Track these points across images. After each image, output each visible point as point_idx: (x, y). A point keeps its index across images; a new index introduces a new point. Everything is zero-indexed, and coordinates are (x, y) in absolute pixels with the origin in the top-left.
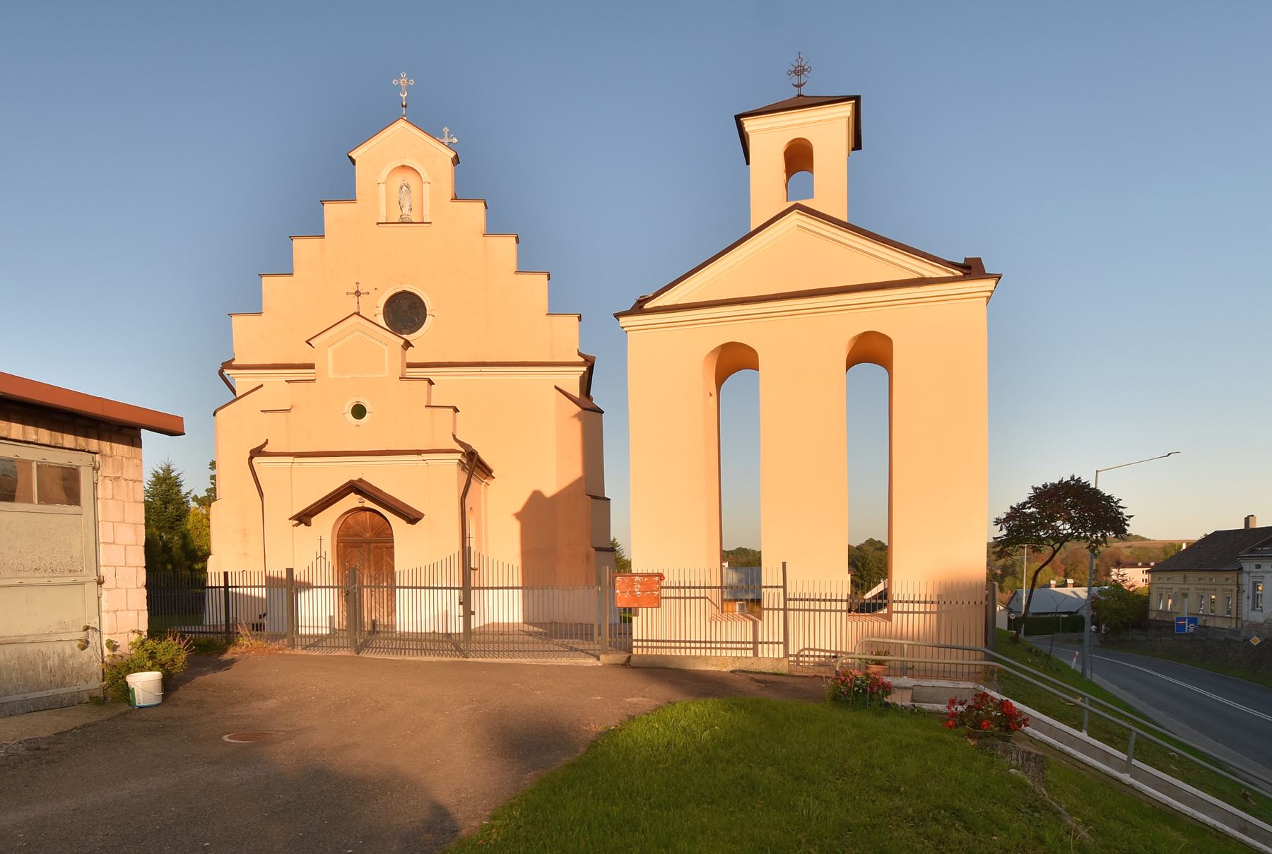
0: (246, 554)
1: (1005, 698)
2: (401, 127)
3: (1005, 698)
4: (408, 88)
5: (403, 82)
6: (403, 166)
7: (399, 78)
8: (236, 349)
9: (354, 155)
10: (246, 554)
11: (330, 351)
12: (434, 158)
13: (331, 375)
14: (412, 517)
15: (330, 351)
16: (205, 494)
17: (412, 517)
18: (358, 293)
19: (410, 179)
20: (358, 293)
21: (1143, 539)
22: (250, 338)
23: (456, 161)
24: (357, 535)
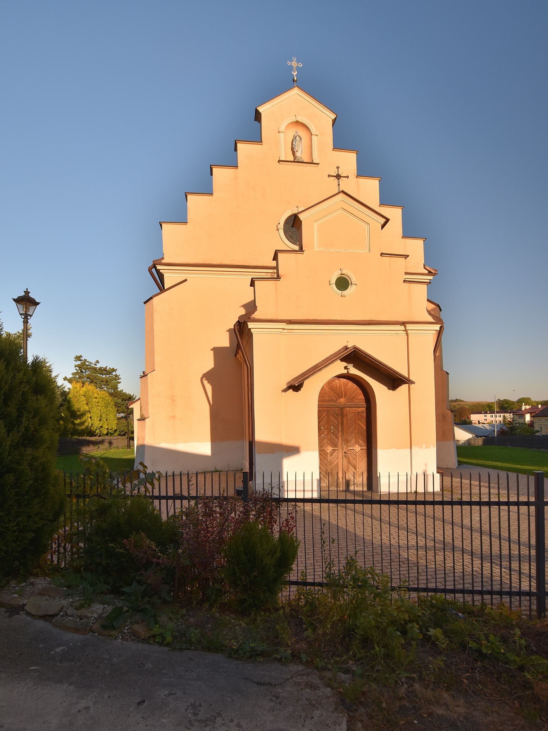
0: (174, 417)
1: (81, 438)
2: (295, 91)
3: (81, 438)
4: (298, 68)
5: (294, 64)
6: (297, 122)
7: (291, 61)
8: (165, 251)
9: (260, 109)
10: (174, 417)
11: (316, 225)
12: (321, 119)
13: (316, 249)
14: (393, 380)
15: (316, 225)
16: (71, 376)
17: (393, 380)
18: (338, 177)
19: (302, 132)
20: (338, 177)
21: (462, 401)
22: (175, 242)
23: (334, 121)
24: (331, 400)
